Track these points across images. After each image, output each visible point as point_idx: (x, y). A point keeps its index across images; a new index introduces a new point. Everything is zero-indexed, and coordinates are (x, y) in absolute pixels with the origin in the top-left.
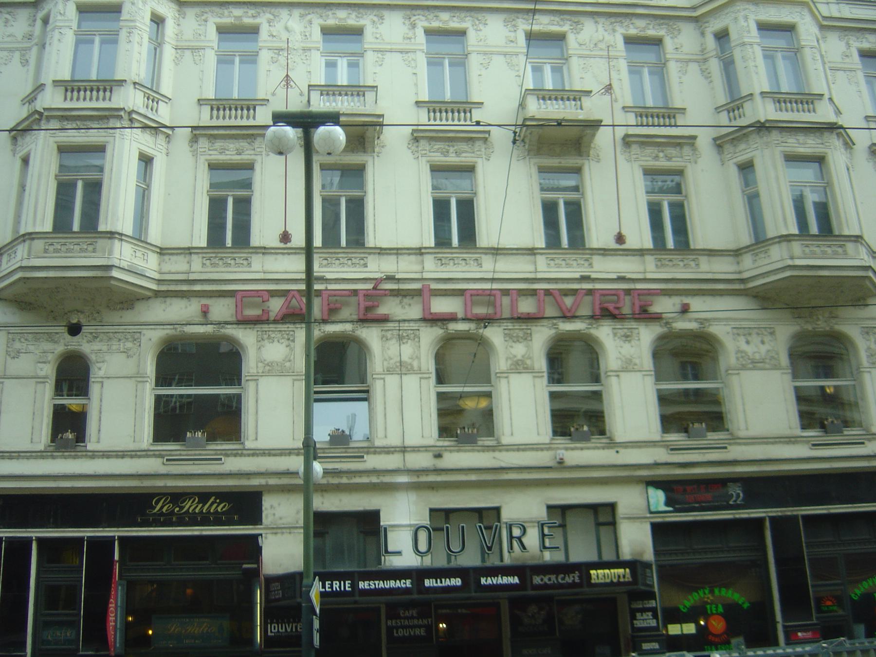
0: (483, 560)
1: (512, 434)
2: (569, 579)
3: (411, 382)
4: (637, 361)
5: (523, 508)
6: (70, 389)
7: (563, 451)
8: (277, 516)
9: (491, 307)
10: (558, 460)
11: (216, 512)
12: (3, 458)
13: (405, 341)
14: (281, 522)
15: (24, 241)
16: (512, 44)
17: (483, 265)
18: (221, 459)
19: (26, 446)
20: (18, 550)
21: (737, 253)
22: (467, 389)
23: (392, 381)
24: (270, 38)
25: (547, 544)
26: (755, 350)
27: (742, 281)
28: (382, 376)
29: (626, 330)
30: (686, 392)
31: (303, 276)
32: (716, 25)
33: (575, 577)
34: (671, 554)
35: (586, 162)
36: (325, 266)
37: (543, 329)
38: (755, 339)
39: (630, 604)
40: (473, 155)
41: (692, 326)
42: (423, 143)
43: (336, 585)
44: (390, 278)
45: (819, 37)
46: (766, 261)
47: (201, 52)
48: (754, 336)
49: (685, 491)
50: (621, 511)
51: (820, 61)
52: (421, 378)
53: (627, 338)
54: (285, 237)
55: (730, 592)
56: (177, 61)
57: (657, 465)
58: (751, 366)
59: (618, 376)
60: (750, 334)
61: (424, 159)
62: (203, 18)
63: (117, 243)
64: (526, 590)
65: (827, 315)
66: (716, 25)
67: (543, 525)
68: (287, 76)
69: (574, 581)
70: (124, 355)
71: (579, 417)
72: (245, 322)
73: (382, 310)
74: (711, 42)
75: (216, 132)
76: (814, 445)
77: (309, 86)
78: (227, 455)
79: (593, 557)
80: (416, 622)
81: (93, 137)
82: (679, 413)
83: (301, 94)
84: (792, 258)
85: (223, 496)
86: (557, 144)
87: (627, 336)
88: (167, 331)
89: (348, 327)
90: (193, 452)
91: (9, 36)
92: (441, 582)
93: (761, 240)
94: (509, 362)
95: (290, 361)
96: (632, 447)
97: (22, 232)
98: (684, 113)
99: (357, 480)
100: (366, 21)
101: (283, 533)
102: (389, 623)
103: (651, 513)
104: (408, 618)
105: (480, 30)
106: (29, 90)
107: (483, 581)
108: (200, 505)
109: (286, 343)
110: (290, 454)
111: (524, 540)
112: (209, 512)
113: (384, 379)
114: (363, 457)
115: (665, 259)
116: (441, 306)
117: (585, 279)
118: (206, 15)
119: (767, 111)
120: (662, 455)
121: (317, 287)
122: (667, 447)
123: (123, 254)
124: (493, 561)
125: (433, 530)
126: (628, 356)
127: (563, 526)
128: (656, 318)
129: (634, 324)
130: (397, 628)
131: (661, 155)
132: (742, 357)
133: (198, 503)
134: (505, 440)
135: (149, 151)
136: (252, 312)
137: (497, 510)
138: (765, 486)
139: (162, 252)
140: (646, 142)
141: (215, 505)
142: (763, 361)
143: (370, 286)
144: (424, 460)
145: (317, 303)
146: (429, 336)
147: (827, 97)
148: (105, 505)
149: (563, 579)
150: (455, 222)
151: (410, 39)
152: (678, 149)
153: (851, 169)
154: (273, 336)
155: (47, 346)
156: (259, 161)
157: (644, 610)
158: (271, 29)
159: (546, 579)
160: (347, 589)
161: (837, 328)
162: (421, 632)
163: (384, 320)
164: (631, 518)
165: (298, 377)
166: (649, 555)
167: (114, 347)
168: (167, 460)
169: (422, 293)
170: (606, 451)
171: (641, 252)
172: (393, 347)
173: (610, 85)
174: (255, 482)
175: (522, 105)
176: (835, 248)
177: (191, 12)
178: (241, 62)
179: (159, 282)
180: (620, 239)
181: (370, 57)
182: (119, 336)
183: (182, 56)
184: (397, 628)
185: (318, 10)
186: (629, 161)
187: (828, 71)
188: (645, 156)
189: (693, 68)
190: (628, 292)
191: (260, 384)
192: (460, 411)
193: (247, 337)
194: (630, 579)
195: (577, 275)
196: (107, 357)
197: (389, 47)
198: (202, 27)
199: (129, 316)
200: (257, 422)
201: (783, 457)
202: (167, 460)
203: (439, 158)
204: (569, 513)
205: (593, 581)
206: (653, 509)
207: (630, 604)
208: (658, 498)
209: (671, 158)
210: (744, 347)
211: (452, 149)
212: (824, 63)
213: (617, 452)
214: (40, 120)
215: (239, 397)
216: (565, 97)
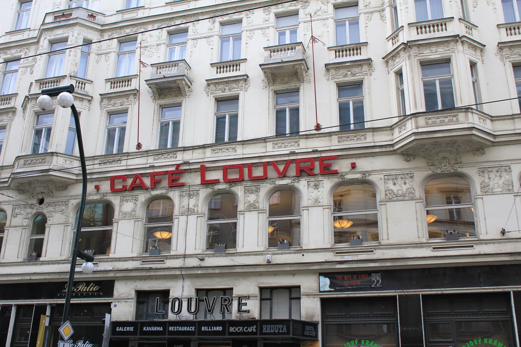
2: (250, 330)
3: (192, 219)
4: (321, 201)
5: (181, 290)
9: (242, 173)
12: (2, 266)
15: (411, 118)
16: (267, 22)
17: (300, 145)
19: (16, 260)
20: (8, 308)
23: (183, 219)
26: (399, 188)
27: (392, 145)
28: (481, 196)
34: (465, 314)
35: (184, 99)
36: (157, 160)
37: (268, 185)
38: (400, 181)
40: (128, 103)
42: (212, 86)
44: (186, 163)
49: (343, 278)
53: (316, 187)
60: (396, 179)
61: (212, 96)
63: (55, 158)
69: (252, 331)
70: (61, 213)
71: (222, 237)
72: (114, 191)
73: (182, 181)
75: (110, 96)
76: (434, 248)
78: (375, 249)
85: (97, 283)
89: (164, 191)
92: (211, 329)
98: (367, 45)
100: (243, 15)
101: (121, 302)
103: (320, 292)
105: (250, 17)
107: (203, 329)
109: (134, 201)
112: (89, 291)
116: (211, 176)
117: (293, 153)
120: (330, 257)
128: (336, 173)
129: (320, 178)
131: (349, 73)
132: (390, 193)
134: (482, 237)
135: (475, 60)
136: (118, 186)
137: (299, 287)
138: (394, 275)
140: (338, 66)
142: (404, 195)
143: (174, 169)
144: (194, 262)
146: (204, 192)
149: (247, 329)
150: (226, 129)
152: (360, 68)
155: (29, 210)
156: (130, 108)
159: (237, 330)
161: (459, 170)
164: (308, 295)
166: (318, 317)
168: (336, 253)
169: (203, 170)
170: (297, 255)
172: (185, 200)
174: (111, 275)
176: (449, 118)
178: (350, 24)
180: (139, 146)
181: (190, 43)
182: (60, 203)
188: (339, 75)
194: (286, 331)
195: (288, 152)
196: (54, 214)
197: (200, 36)
199: (65, 193)
202: (336, 253)
203: (220, 94)
206: (322, 290)
208: (325, 282)
209: (355, 74)
210: (391, 186)
211: (227, 88)
213: (303, 255)
216: (286, 48)
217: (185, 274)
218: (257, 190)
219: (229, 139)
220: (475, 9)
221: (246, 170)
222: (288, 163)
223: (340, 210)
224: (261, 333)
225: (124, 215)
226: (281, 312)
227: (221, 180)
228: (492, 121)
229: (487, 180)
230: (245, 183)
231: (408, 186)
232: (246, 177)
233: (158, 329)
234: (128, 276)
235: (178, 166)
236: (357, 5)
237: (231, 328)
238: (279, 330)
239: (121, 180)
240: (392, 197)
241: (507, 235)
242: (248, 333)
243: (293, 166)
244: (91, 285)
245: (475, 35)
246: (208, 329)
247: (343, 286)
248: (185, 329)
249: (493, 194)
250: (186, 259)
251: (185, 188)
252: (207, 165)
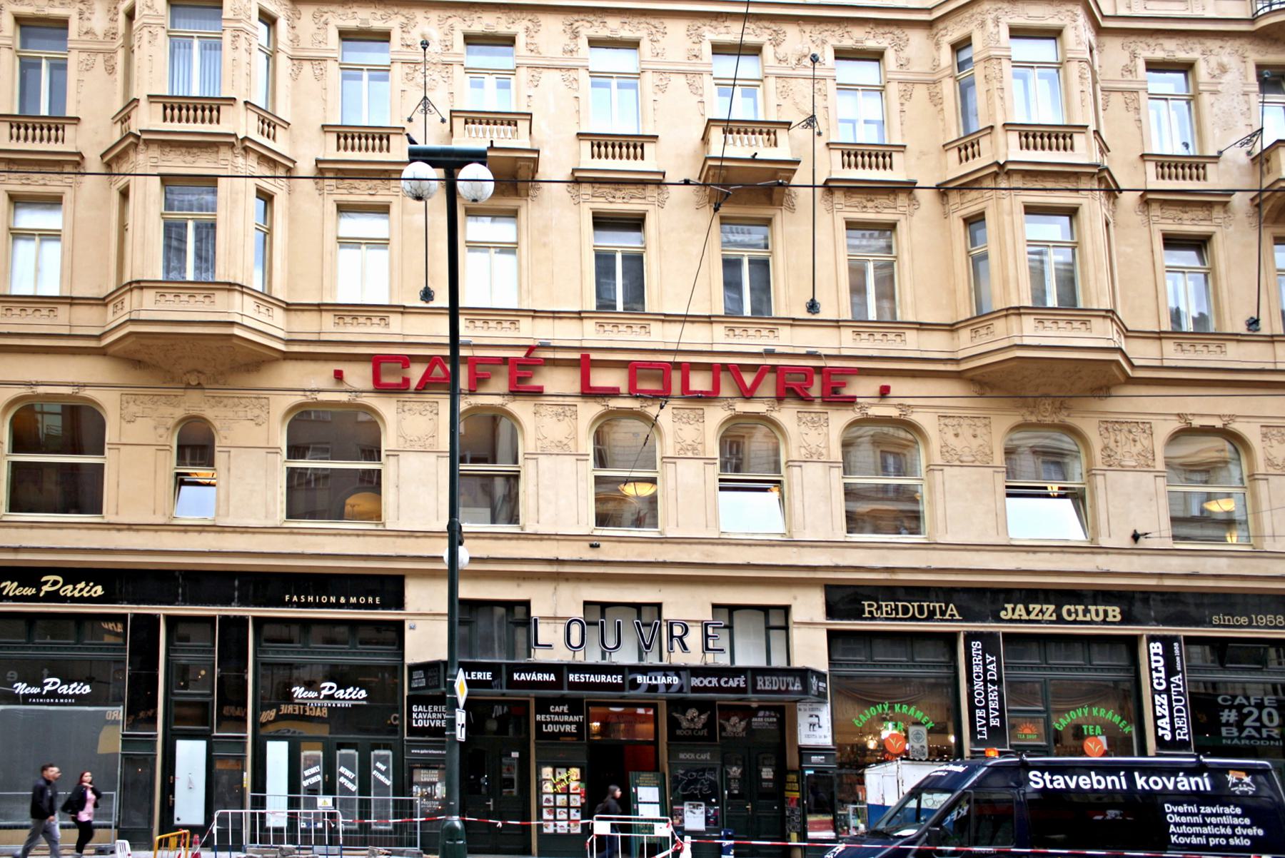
0: (641, 658)
2: (733, 683)
6: (193, 458)
15: (131, 290)
16: (695, 60)
21: (952, 328)
22: (633, 474)
24: (405, 49)
25: (711, 646)
30: (885, 488)
31: (447, 341)
32: (954, 32)
33: (739, 682)
38: (966, 431)
43: (480, 675)
45: (1094, 45)
47: (323, 64)
48: (965, 427)
50: (796, 616)
51: (1090, 80)
54: (427, 295)
55: (913, 709)
56: (295, 77)
62: (323, 19)
63: (237, 295)
65: (1057, 404)
66: (954, 32)
67: (706, 625)
68: (425, 98)
72: (381, 388)
74: (946, 56)
77: (451, 111)
79: (760, 662)
80: (566, 718)
81: (201, 165)
82: (873, 510)
83: (443, 121)
86: (745, 191)
88: (298, 398)
89: (496, 401)
91: (87, 33)
93: (985, 311)
97: (127, 279)
100: (516, 26)
102: (538, 717)
106: (119, 105)
107: (516, 676)
109: (430, 416)
111: (685, 639)
116: (601, 379)
117: (770, 353)
118: (326, 16)
119: (1011, 150)
121: (463, 352)
123: (241, 309)
124: (651, 659)
125: (586, 624)
127: (730, 627)
128: (851, 401)
137: (659, 606)
139: (289, 307)
143: (521, 354)
145: (463, 372)
146: (590, 411)
147: (1092, 127)
148: (236, 583)
149: (726, 682)
151: (571, 51)
153: (1111, 226)
158: (405, 36)
159: (706, 682)
162: (573, 728)
163: (538, 392)
167: (241, 414)
169: (584, 363)
171: (837, 324)
173: (813, 116)
175: (705, 139)
177: (307, 11)
179: (288, 342)
180: (813, 306)
183: (300, 69)
184: (547, 723)
185: (460, 12)
186: (831, 210)
187: (1099, 93)
189: (920, 92)
190: (819, 370)
191: (401, 462)
192: (623, 499)
193: (386, 407)
198: (322, 32)
204: (736, 614)
212: (1095, 82)
214: (137, 145)
215: (101, 466)
217: (557, 574)
219: (753, 311)
220: (659, 96)
221: (676, 377)
222: (761, 371)
223: (737, 469)
224: (755, 691)
226: (749, 655)
227: (624, 389)
228: (1126, 337)
229: (1112, 445)
230: (673, 403)
231: (979, 441)
232: (676, 388)
233: (546, 677)
235: (531, 349)
236: (388, 41)
239: (400, 365)
240: (953, 460)
241: (1143, 543)
242: (731, 690)
243: (770, 379)
245: (281, 145)
248: (603, 678)
249: (1123, 468)
252: (594, 356)
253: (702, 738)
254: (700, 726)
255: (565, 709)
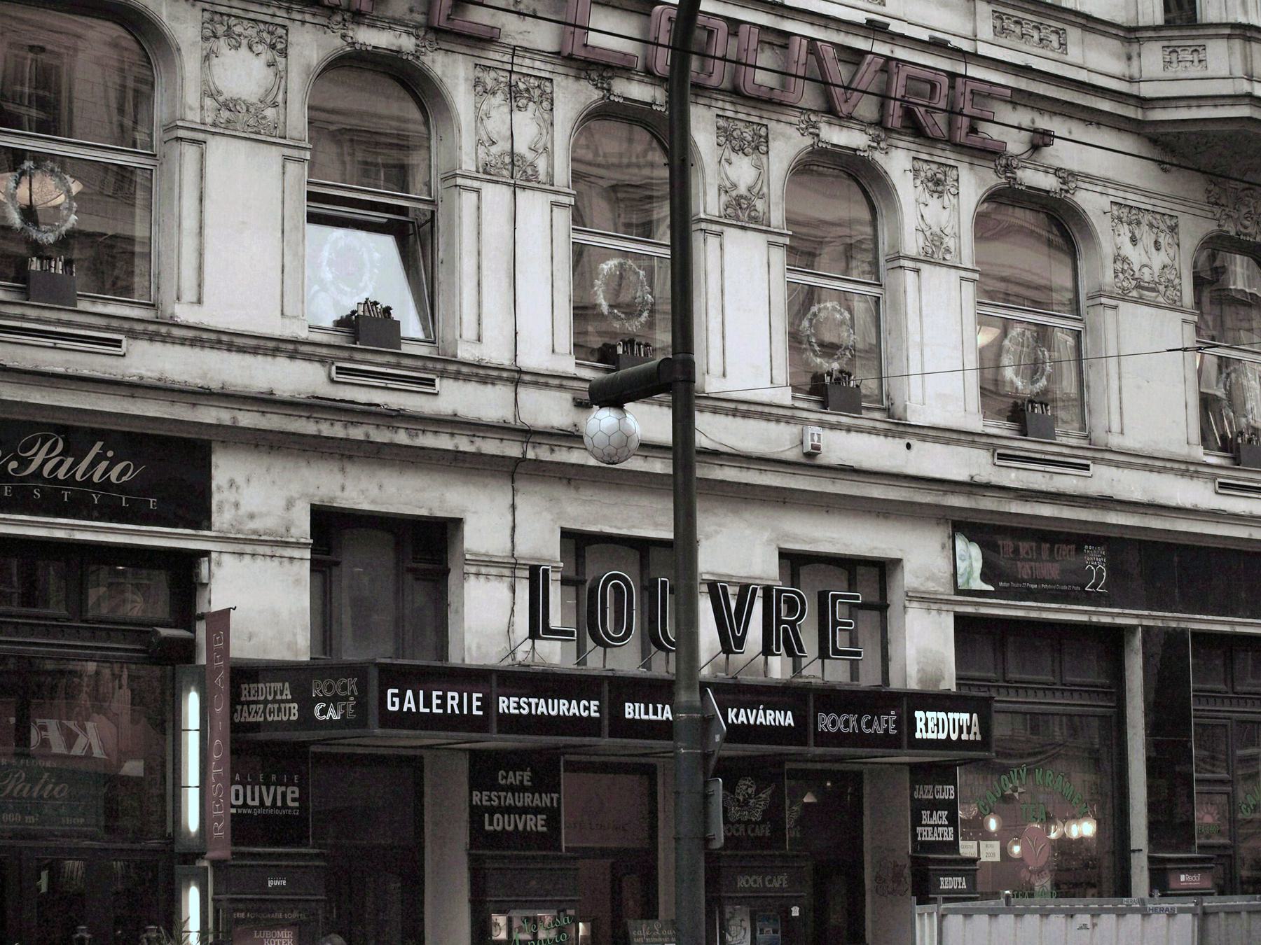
1: (724, 375)
7: (817, 430)
8: (243, 510)
10: (808, 448)
11: (106, 485)
13: (522, 102)
14: (252, 525)
18: (117, 343)
26: (1145, 260)
28: (476, 184)
29: (934, 167)
33: (885, 724)
38: (1147, 238)
39: (913, 789)
41: (1048, 182)
46: (1195, 71)
52: (553, 204)
57: (972, 487)
58: (1134, 293)
59: (918, 271)
64: (805, 744)
69: (887, 730)
76: (1222, 485)
78: (132, 335)
80: (527, 799)
84: (1250, 78)
87: (938, 183)
89: (407, 43)
90: (47, 314)
92: (655, 713)
94: (724, 198)
95: (275, 105)
96: (935, 440)
99: (428, 441)
104: (512, 789)
108: (69, 461)
109: (267, 55)
110: (275, 352)
112: (88, 482)
113: (478, 191)
114: (431, 383)
115: (1009, 17)
122: (993, 449)
126: (936, 229)
128: (990, 154)
129: (949, 157)
130: (492, 811)
133: (64, 453)
141: (104, 464)
146: (572, 97)
154: (238, 29)
157: (935, 805)
160: (475, 712)
162: (536, 824)
163: (482, 40)
164: (927, 600)
165: (295, 153)
174: (210, 415)
184: (492, 811)
194: (979, 737)
195: (860, 18)
200: (201, 255)
201: (1173, 503)
202: (340, 370)
205: (918, 735)
207: (913, 789)
208: (971, 556)
210: (1128, 250)
213: (909, 446)
218: (759, 145)
225: (225, 114)
234: (285, 434)
237: (821, 716)
238: (275, 693)
244: (97, 448)
246: (647, 713)
247: (1016, 580)
248: (562, 707)
250: (521, 390)
251: (495, 56)
253: (760, 842)
254: (757, 816)
255: (526, 777)
